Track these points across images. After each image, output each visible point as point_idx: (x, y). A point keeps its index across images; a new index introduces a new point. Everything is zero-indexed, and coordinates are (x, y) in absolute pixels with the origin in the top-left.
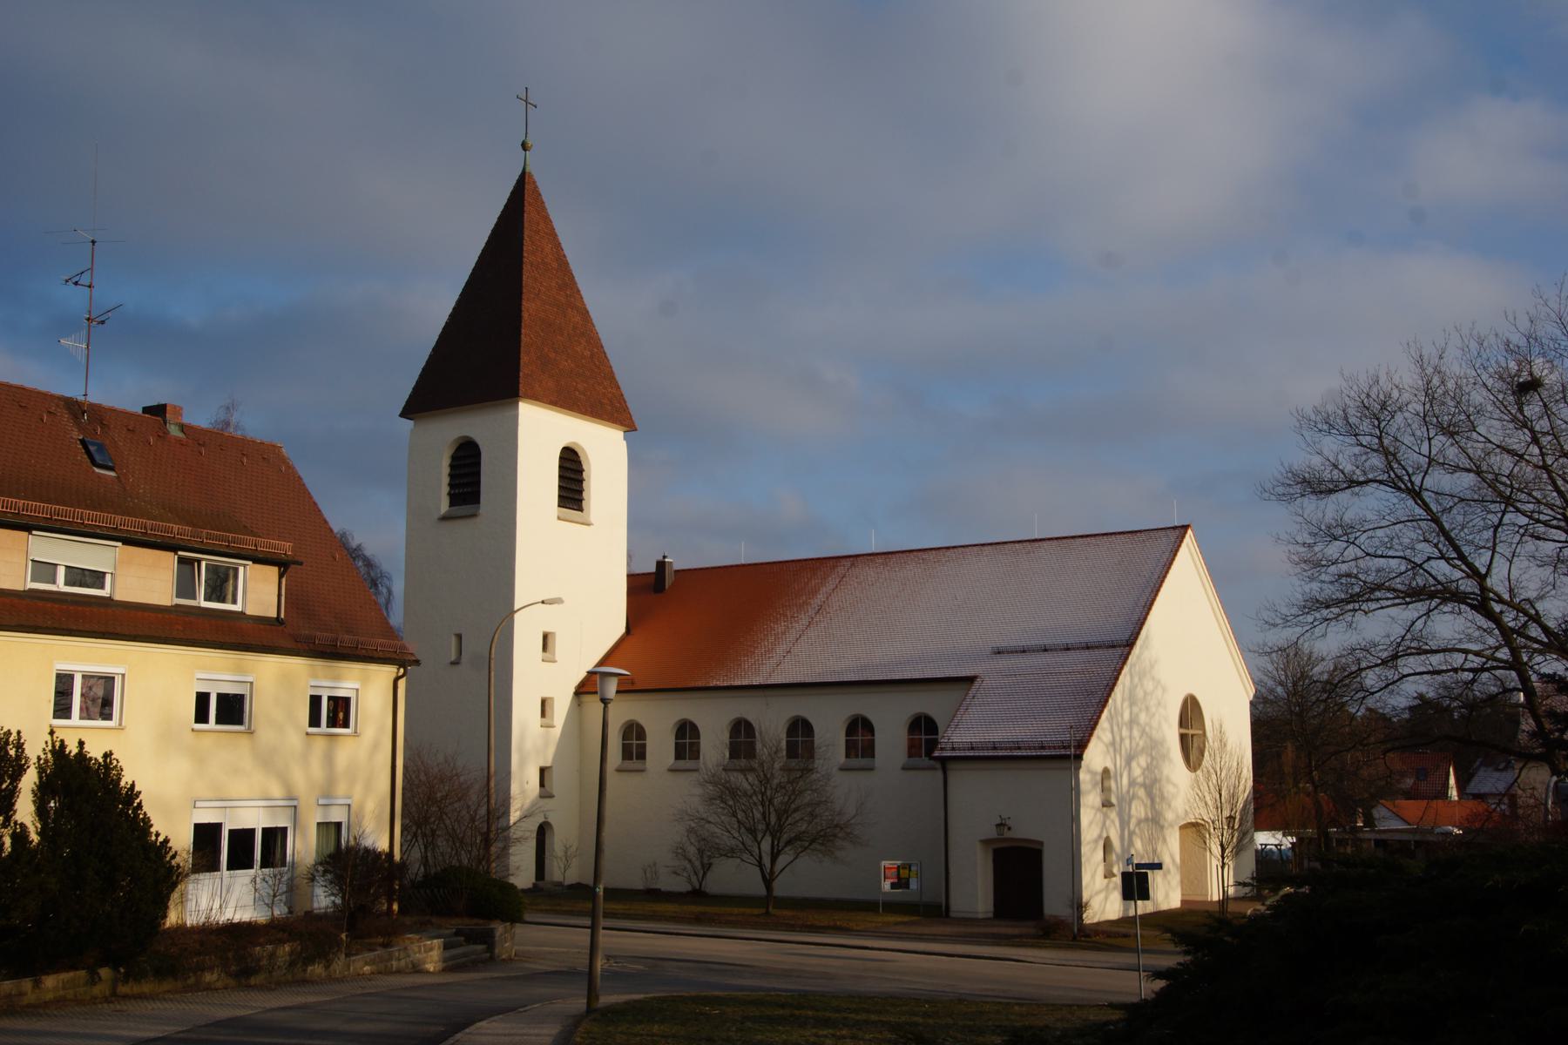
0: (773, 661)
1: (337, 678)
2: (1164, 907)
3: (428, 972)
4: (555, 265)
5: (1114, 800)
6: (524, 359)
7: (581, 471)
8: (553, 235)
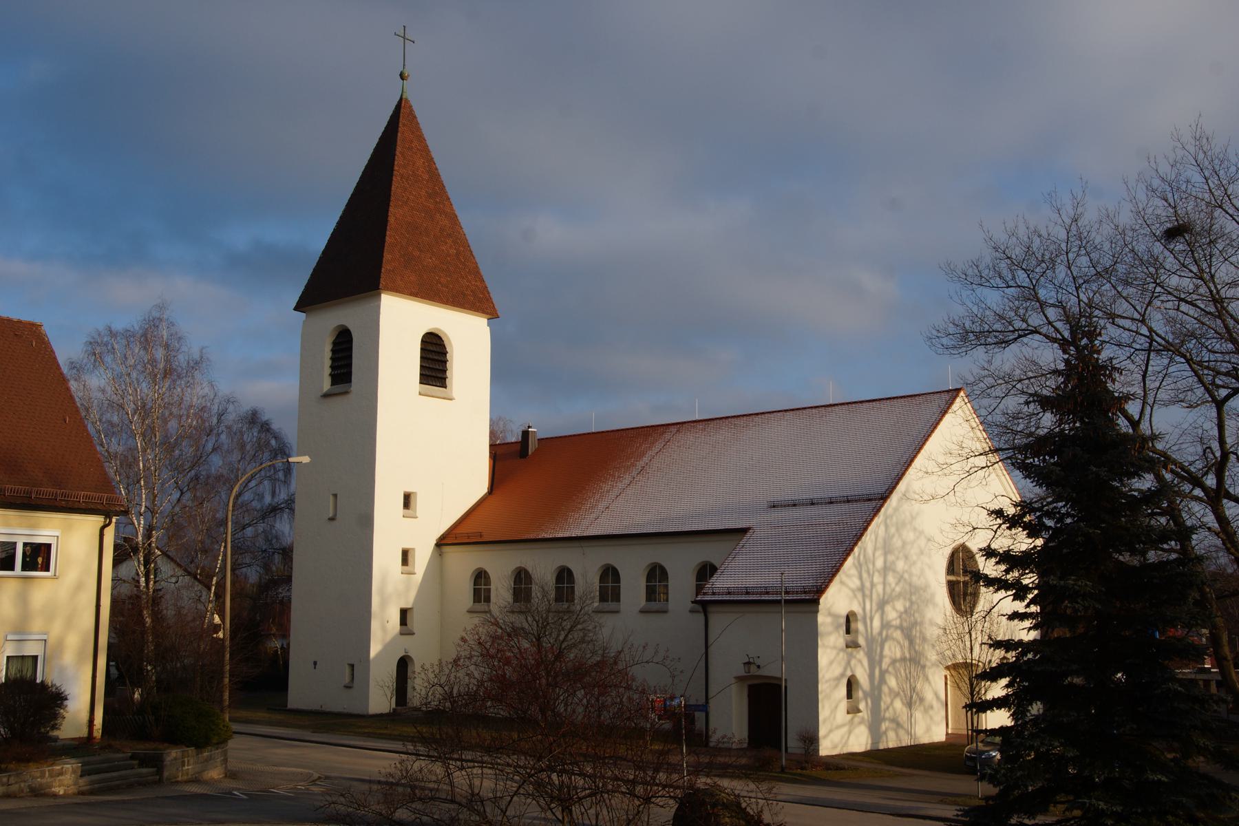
0: (594, 515)
1: (34, 526)
2: (925, 740)
3: (55, 796)
5: (861, 641)
6: (387, 256)
7: (445, 353)
8: (425, 151)
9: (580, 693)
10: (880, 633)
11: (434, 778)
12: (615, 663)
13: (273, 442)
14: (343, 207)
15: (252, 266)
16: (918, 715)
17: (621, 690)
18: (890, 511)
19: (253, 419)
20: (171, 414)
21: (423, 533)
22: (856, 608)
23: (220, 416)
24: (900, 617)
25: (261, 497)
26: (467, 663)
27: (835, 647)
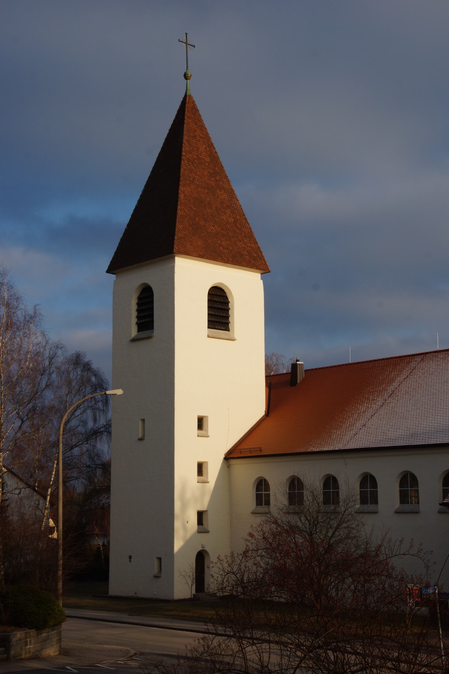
0: (352, 433)
4: (208, 159)
6: (179, 226)
9: (349, 580)
11: (230, 653)
12: (377, 555)
13: (93, 379)
14: (142, 188)
15: (71, 237)
17: (383, 577)
19: (77, 361)
20: (13, 359)
23: (51, 359)
25: (85, 423)
26: (255, 555)
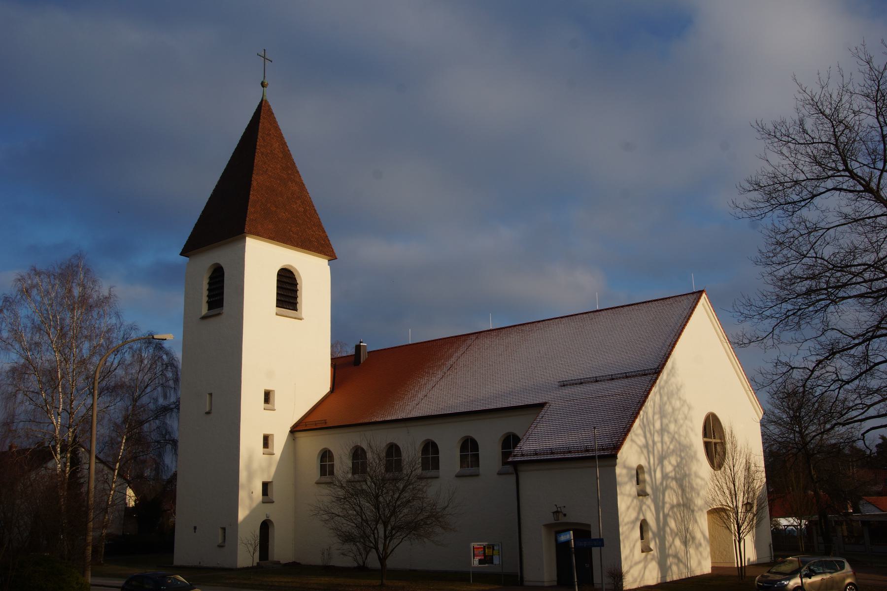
2: (698, 573)
4: (281, 155)
5: (649, 490)
6: (251, 209)
10: (662, 483)
13: (165, 357)
16: (692, 551)
18: (662, 383)
19: (150, 340)
21: (280, 422)
22: (643, 462)
24: (674, 469)
25: (156, 400)
27: (630, 495)
